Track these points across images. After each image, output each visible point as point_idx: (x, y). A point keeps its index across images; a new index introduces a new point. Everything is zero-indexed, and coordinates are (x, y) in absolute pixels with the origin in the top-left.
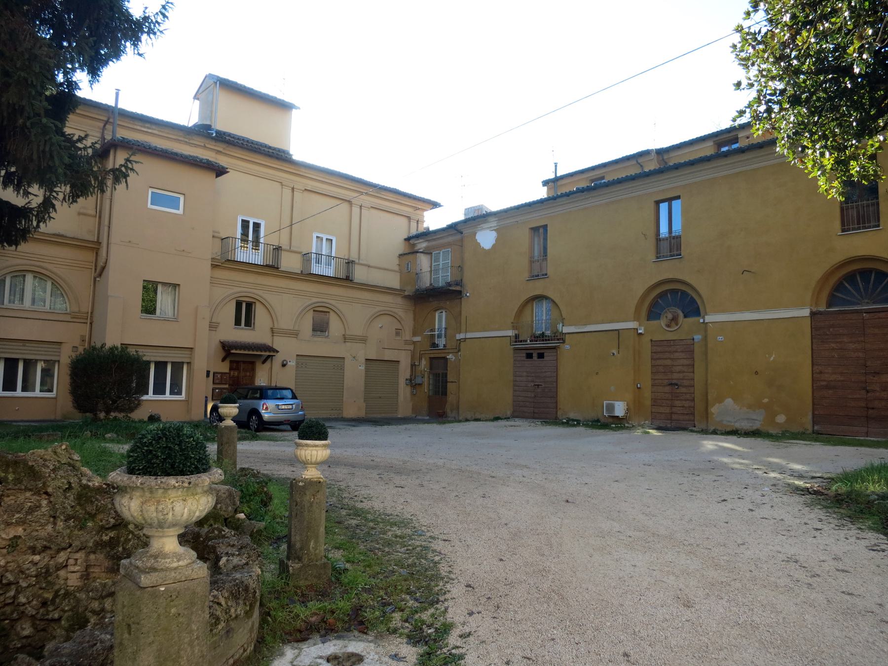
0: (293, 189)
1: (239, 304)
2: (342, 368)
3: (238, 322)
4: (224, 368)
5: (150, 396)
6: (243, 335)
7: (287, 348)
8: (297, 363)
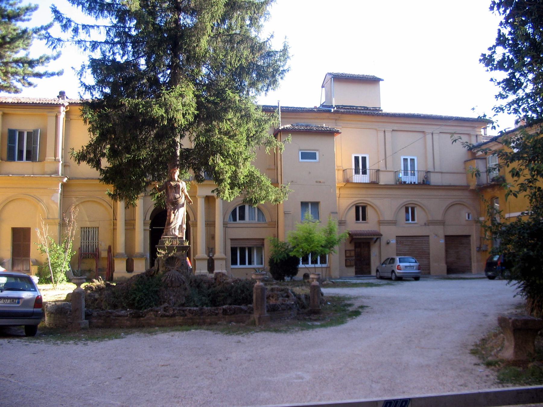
0: (384, 131)
1: (357, 208)
2: (428, 243)
3: (357, 219)
4: (351, 247)
5: (301, 265)
6: (361, 227)
7: (389, 234)
8: (397, 243)
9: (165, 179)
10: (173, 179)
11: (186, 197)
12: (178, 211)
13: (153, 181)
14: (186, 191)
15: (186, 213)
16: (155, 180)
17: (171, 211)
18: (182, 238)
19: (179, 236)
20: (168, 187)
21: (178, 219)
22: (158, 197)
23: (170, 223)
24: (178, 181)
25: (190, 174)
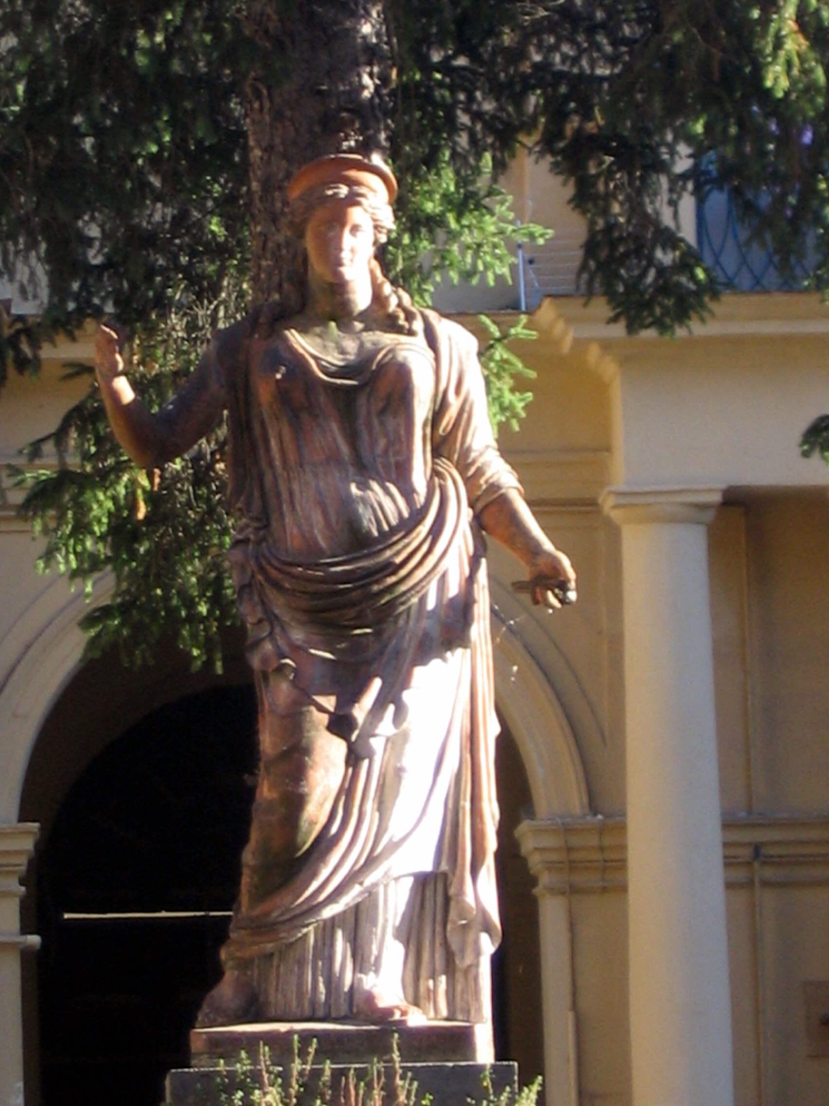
9: (205, 289)
10: (315, 298)
11: (491, 516)
12: (391, 696)
13: (61, 323)
14: (482, 437)
15: (490, 729)
16: (89, 309)
17: (304, 697)
18: (458, 1040)
19: (417, 1019)
20: (264, 393)
21: (398, 789)
22: (123, 531)
23: (294, 862)
24: (382, 318)
25: (522, 217)
